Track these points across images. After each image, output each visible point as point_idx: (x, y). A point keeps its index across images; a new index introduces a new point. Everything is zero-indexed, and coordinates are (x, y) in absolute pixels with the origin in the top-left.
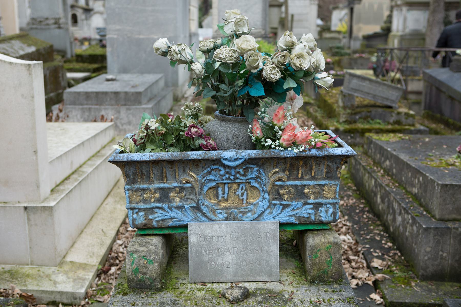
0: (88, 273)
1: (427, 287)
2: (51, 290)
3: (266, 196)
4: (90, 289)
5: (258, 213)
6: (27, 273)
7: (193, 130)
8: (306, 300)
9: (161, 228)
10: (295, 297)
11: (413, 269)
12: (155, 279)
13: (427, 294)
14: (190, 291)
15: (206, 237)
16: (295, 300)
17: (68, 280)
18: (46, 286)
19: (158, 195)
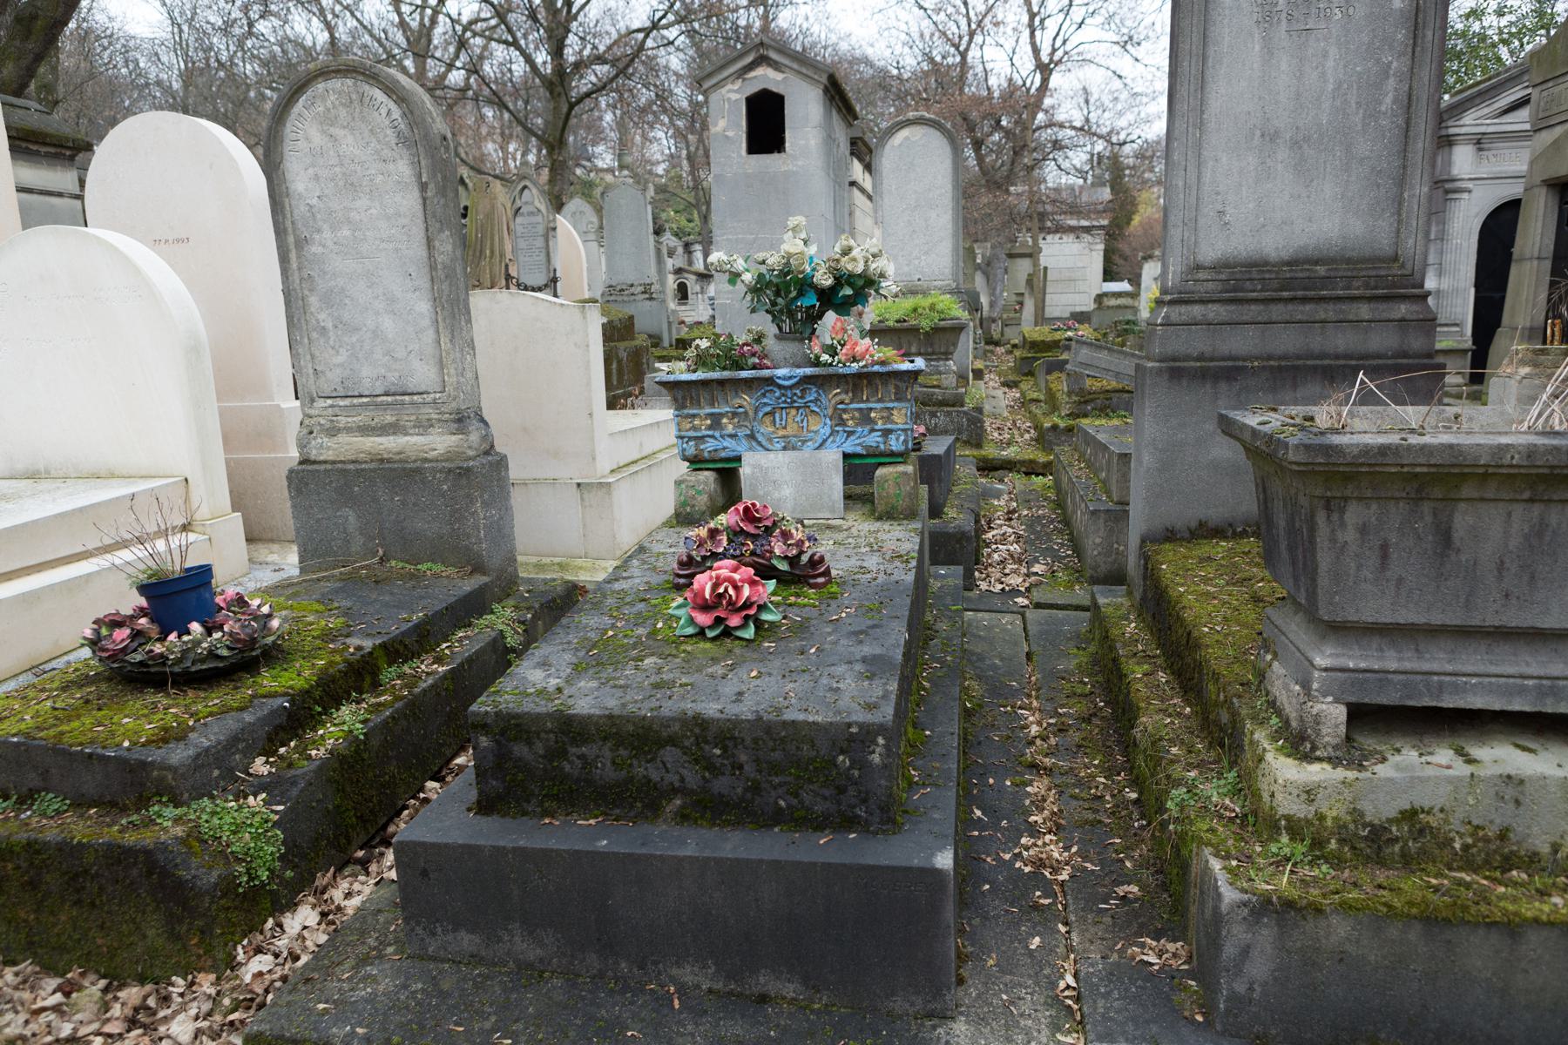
3: (828, 421)
5: (820, 441)
7: (746, 348)
9: (714, 461)
19: (709, 422)
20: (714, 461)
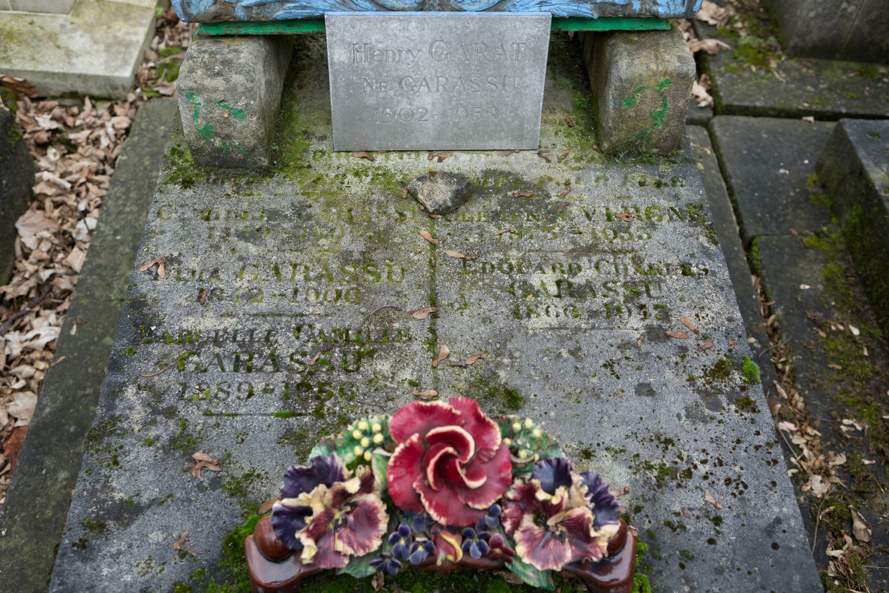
0: (136, 29)
1: (799, 70)
2: (61, 71)
4: (144, 65)
6: (7, 28)
8: (597, 210)
9: (260, 23)
10: (572, 201)
11: (776, 30)
12: (253, 149)
13: (798, 88)
14: (337, 176)
15: (370, 50)
16: (574, 210)
17: (96, 47)
18: (50, 61)
20: (260, 23)
